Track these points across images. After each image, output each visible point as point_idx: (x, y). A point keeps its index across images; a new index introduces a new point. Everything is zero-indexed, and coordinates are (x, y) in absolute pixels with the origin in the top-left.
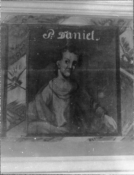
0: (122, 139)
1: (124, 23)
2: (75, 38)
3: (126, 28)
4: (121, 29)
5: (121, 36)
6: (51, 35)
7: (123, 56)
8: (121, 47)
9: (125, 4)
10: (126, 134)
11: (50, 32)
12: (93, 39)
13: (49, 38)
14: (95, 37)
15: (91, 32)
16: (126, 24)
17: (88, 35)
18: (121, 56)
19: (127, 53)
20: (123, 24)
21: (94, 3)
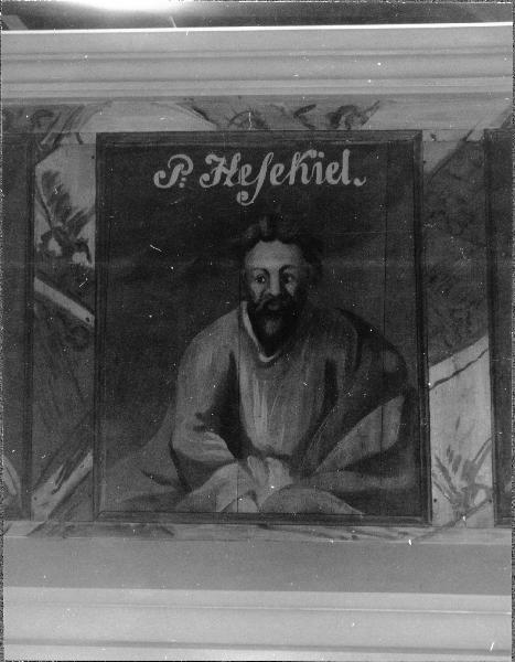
0: (32, 529)
1: (54, 119)
2: (292, 182)
3: (59, 137)
4: (44, 142)
5: (41, 169)
6: (180, 175)
7: (46, 238)
8: (40, 207)
9: (273, 54)
10: (48, 511)
11: (177, 164)
12: (346, 182)
13: (173, 187)
14: (352, 174)
15: (339, 159)
16: (61, 123)
17: (330, 172)
18: (39, 238)
19: (60, 224)
20: (52, 125)
21: (319, 68)
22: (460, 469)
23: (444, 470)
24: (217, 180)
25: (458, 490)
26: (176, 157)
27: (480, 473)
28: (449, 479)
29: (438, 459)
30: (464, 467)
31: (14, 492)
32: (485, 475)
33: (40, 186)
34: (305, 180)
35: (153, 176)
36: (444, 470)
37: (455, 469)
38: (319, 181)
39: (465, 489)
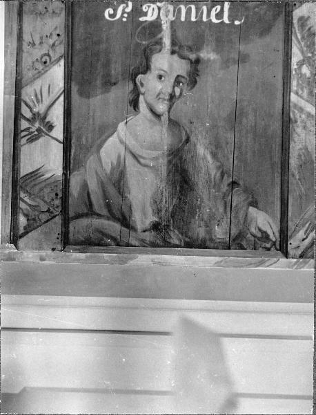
2: (183, 19)
6: (124, 12)
7: (300, 64)
13: (118, 19)
17: (213, 13)
24: (118, 16)
31: (274, 240)
33: (297, 28)
35: (104, 12)
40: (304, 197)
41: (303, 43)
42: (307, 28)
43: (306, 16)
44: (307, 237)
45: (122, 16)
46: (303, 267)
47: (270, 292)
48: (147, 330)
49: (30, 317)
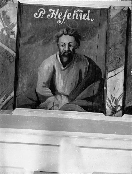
6: (42, 15)
14: (90, 18)
17: (84, 16)
22: (114, 101)
23: (110, 101)
24: (52, 16)
25: (113, 106)
26: (40, 9)
27: (119, 102)
28: (111, 103)
29: (108, 98)
30: (115, 100)
32: (120, 103)
34: (77, 18)
36: (110, 101)
37: (113, 101)
38: (81, 19)
39: (115, 106)
40: (3, 84)
41: (4, 22)
42: (6, 15)
43: (5, 11)
44: (4, 101)
45: (41, 16)
46: (2, 113)
47: (100, 139)
48: (32, 146)
49: (10, 138)
